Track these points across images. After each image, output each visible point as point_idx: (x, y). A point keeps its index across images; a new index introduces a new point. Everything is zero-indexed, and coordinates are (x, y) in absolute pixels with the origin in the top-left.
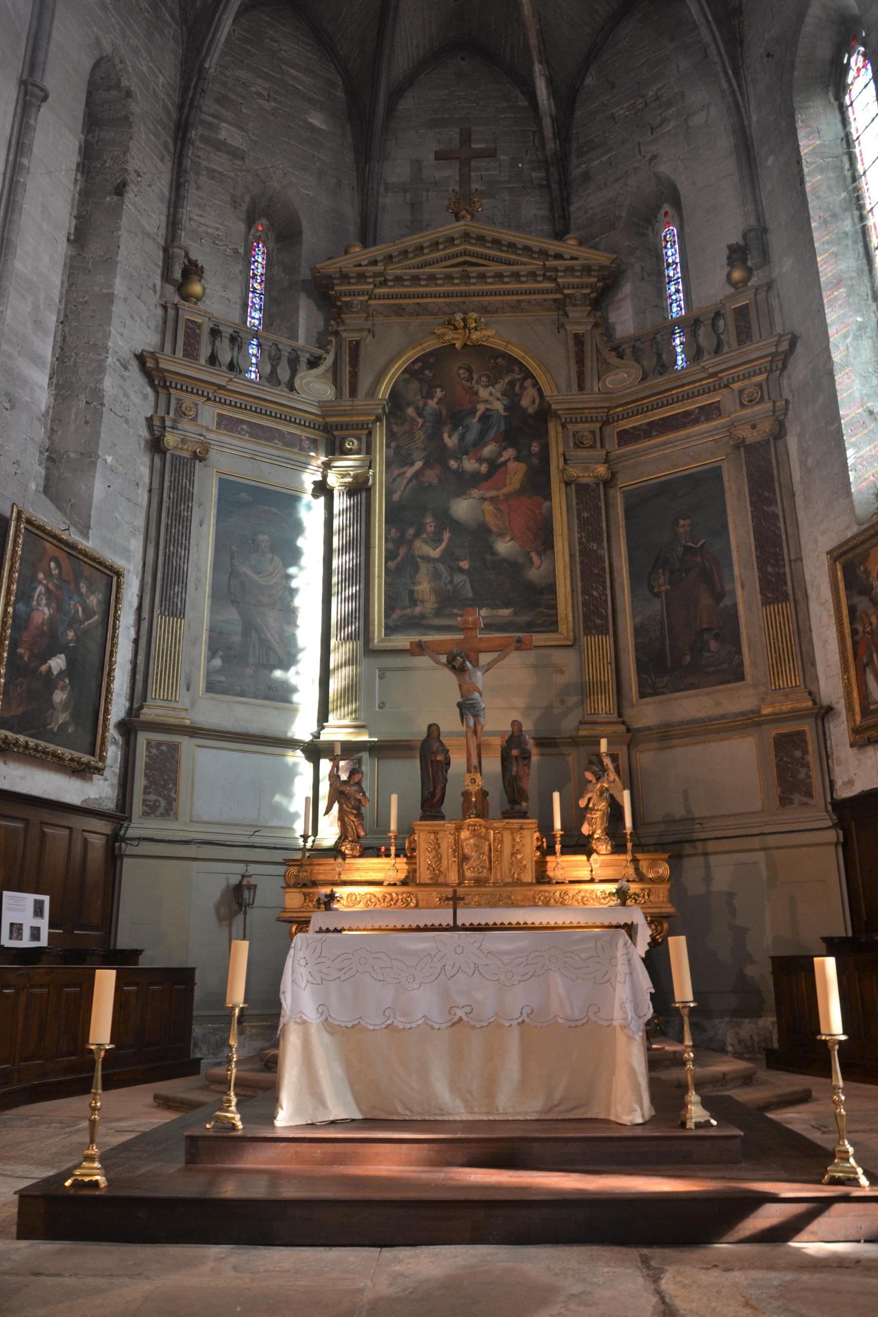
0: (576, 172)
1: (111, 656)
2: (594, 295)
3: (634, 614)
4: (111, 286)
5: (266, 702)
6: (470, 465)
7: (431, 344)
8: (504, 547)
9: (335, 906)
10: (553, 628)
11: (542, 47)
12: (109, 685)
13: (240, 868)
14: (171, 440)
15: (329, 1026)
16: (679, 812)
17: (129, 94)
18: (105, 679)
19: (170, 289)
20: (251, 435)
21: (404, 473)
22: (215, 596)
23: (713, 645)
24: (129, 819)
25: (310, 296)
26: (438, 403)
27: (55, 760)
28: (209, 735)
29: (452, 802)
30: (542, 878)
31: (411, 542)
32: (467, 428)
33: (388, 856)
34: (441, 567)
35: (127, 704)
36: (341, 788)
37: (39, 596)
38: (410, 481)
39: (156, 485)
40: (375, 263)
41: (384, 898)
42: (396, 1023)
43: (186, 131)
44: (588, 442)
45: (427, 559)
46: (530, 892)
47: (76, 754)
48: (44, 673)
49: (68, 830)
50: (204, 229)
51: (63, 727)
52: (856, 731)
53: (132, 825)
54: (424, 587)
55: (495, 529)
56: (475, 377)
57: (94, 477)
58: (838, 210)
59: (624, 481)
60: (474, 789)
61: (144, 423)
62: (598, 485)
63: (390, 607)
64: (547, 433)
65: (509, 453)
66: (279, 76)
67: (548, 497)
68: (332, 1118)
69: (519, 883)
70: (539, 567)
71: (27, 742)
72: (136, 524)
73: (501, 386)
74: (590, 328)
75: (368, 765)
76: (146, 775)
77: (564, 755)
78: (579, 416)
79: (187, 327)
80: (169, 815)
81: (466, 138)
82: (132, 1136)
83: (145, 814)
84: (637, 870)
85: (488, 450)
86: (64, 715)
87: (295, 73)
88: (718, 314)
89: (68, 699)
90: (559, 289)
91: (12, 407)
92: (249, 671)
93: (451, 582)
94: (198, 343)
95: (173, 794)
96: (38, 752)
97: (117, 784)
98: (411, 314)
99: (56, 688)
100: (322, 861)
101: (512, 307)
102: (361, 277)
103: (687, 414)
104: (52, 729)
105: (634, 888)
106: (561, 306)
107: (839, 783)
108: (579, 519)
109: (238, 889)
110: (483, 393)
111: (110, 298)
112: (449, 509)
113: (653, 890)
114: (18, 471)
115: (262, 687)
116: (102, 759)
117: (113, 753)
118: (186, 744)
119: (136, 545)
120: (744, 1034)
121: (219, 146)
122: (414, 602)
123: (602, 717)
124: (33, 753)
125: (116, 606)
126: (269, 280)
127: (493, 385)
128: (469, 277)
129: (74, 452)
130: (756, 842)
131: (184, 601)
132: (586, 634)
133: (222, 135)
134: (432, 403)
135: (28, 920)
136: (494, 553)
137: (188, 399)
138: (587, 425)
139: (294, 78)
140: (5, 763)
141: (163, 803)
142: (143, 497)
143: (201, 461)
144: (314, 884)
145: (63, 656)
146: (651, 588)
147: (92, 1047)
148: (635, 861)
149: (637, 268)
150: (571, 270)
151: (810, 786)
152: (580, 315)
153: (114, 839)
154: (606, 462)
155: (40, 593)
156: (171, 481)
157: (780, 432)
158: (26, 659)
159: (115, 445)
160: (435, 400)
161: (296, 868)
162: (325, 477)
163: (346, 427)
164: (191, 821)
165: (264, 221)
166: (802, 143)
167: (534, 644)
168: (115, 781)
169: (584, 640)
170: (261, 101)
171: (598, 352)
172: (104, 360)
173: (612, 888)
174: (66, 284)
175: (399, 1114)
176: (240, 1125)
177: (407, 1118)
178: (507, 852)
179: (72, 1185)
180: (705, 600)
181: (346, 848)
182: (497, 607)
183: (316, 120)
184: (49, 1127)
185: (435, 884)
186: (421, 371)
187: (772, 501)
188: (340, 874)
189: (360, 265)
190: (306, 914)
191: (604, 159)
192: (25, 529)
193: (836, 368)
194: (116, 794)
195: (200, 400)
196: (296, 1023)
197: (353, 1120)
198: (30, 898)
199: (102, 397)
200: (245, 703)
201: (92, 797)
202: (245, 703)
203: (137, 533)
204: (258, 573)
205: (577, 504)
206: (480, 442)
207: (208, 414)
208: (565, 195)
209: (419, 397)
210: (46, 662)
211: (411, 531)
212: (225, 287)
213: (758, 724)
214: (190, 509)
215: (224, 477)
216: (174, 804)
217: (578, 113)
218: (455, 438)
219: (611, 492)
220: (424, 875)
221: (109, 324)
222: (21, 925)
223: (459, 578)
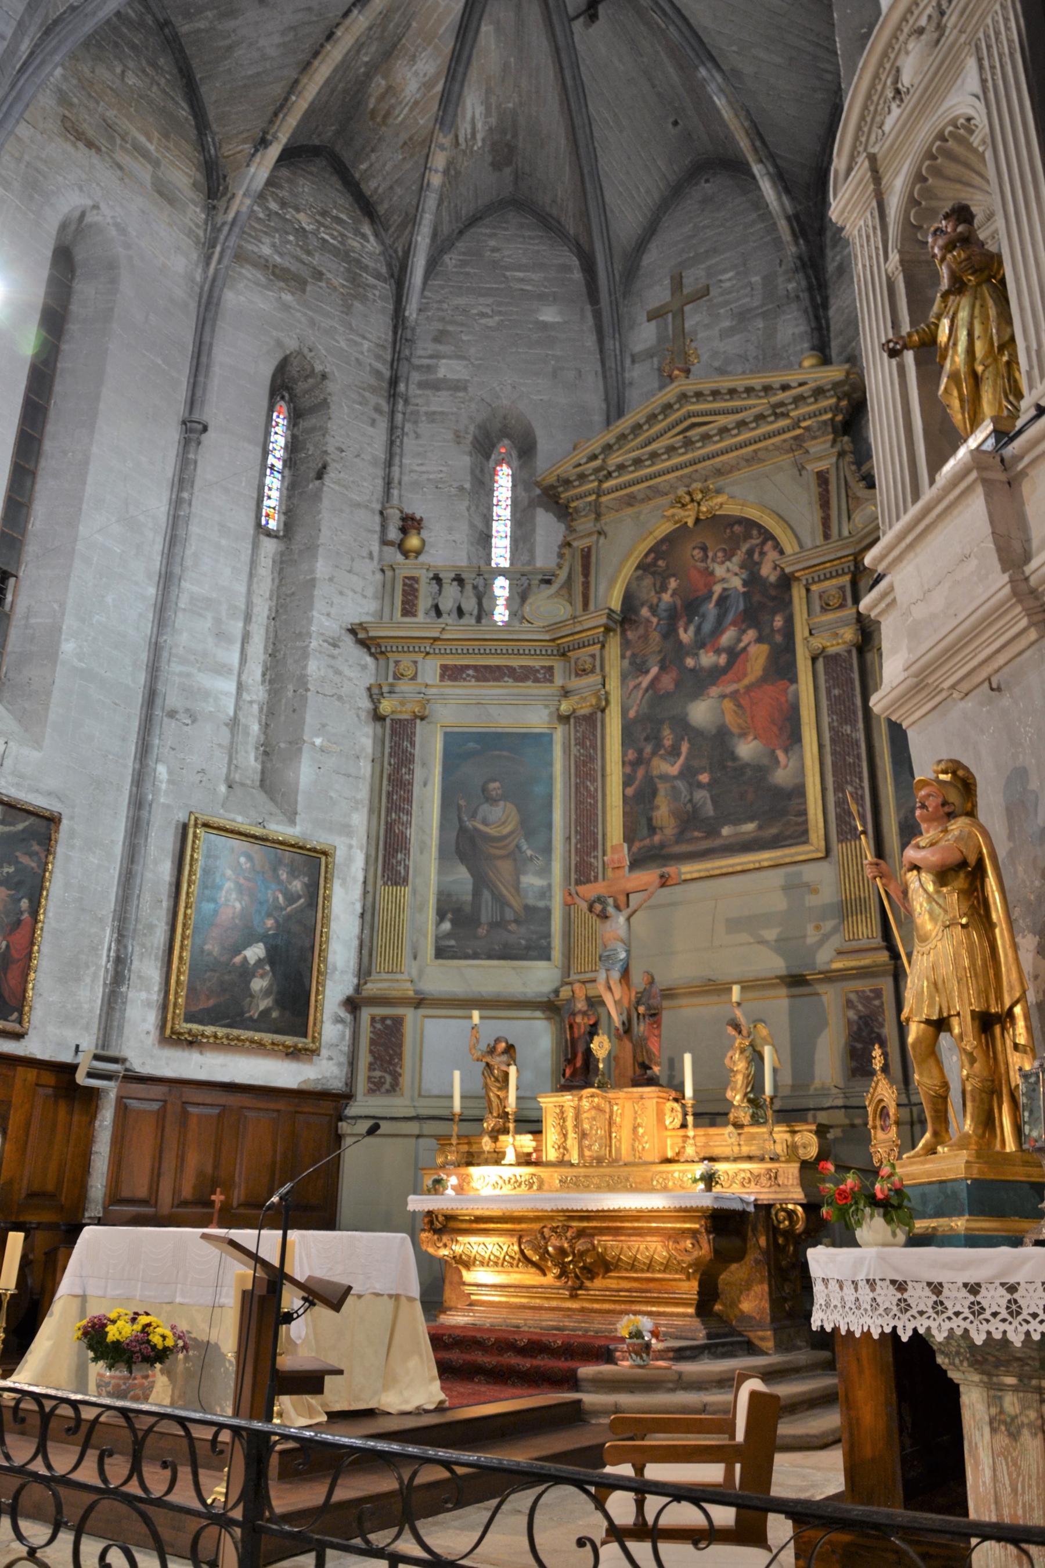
2: (839, 418)
4: (312, 571)
6: (707, 659)
8: (746, 749)
10: (803, 839)
11: (758, 144)
17: (324, 376)
20: (478, 680)
21: (640, 684)
26: (672, 596)
31: (649, 761)
32: (703, 616)
34: (680, 784)
38: (647, 690)
40: (594, 457)
45: (664, 777)
50: (425, 476)
51: (266, 1013)
55: (735, 730)
56: (710, 554)
61: (365, 694)
62: (849, 652)
64: (790, 602)
65: (751, 634)
66: (503, 286)
67: (794, 680)
70: (786, 766)
72: (359, 797)
74: (834, 460)
76: (371, 1051)
77: (818, 994)
78: (821, 573)
79: (405, 584)
83: (371, 1091)
85: (727, 637)
87: (520, 275)
89: (271, 985)
91: (193, 722)
93: (691, 801)
94: (416, 597)
98: (642, 501)
99: (254, 976)
101: (747, 460)
102: (582, 477)
104: (251, 1017)
108: (829, 698)
110: (720, 571)
111: (312, 583)
112: (687, 714)
113: (780, 1173)
118: (409, 1014)
121: (436, 386)
124: (225, 1042)
127: (729, 559)
128: (693, 443)
131: (406, 868)
132: (840, 841)
133: (442, 372)
134: (666, 597)
136: (734, 757)
137: (406, 660)
138: (834, 582)
139: (522, 280)
140: (201, 1053)
141: (389, 1079)
150: (799, 400)
152: (823, 447)
159: (324, 726)
160: (670, 592)
164: (420, 1095)
165: (506, 442)
167: (683, 877)
170: (484, 321)
172: (308, 646)
173: (699, 1169)
174: (277, 581)
185: (561, 1163)
186: (654, 563)
189: (580, 465)
195: (419, 657)
199: (306, 683)
205: (826, 681)
206: (718, 629)
208: (819, 300)
209: (653, 593)
211: (648, 749)
212: (450, 530)
214: (411, 772)
215: (449, 730)
218: (692, 629)
221: (311, 609)
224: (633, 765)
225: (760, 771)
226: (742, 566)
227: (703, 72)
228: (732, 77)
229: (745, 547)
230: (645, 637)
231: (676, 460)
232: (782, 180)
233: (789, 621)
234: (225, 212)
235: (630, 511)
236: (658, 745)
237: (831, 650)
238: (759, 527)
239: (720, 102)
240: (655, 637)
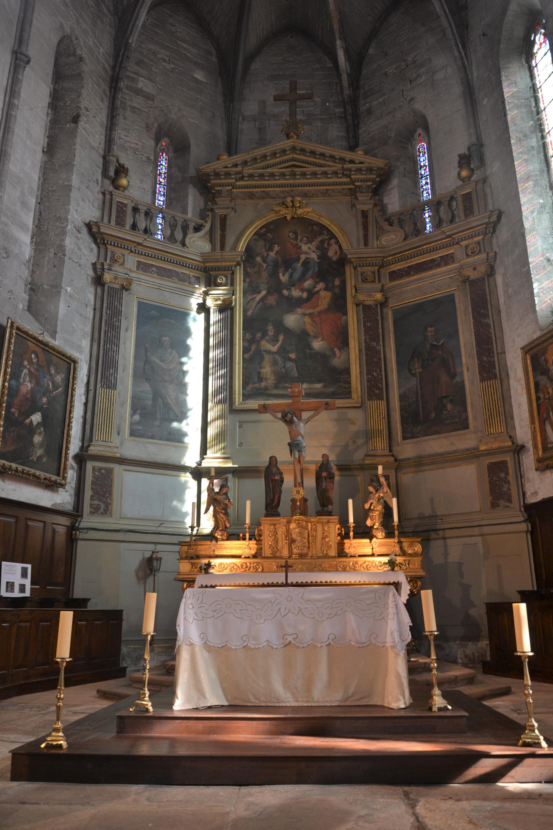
0: (363, 109)
1: (70, 413)
2: (374, 186)
3: (400, 387)
4: (70, 180)
5: (168, 443)
6: (296, 293)
7: (272, 217)
8: (317, 345)
9: (211, 571)
10: (348, 396)
11: (341, 29)
12: (68, 432)
13: (151, 547)
14: (107, 277)
15: (207, 646)
16: (428, 512)
17: (81, 59)
18: (66, 428)
19: (107, 182)
20: (158, 274)
21: (255, 298)
22: (136, 375)
23: (449, 406)
24: (81, 516)
25: (195, 186)
26: (276, 254)
27: (35, 479)
28: (132, 463)
29: (285, 506)
30: (342, 553)
31: (259, 342)
32: (294, 270)
33: (244, 539)
34: (278, 357)
35: (80, 444)
36: (215, 497)
37: (24, 376)
38: (258, 303)
39: (98, 306)
40: (236, 165)
41: (242, 566)
42: (249, 645)
43: (117, 82)
44: (370, 279)
45: (269, 352)
46: (334, 562)
47: (48, 475)
48: (27, 424)
49: (43, 523)
50: (129, 144)
51: (40, 458)
52: (539, 461)
53: (83, 520)
54: (267, 370)
55: (312, 334)
56: (299, 237)
57: (59, 300)
58: (528, 132)
59: (393, 303)
60: (298, 497)
61: (90, 266)
62: (376, 305)
63: (245, 383)
64: (344, 273)
65: (321, 285)
66: (176, 48)
67: (345, 313)
68: (209, 705)
69: (327, 557)
70: (340, 357)
71: (17, 468)
72: (86, 330)
73: (315, 243)
74: (371, 206)
75: (232, 482)
76: (92, 489)
77: (355, 476)
78: (364, 262)
79: (118, 206)
80: (106, 514)
81: (293, 87)
82: (83, 716)
83: (92, 513)
84: (401, 548)
85: (308, 284)
86: (40, 451)
87: (186, 46)
88: (452, 198)
89: (43, 440)
90: (352, 182)
91: (8, 257)
92: (157, 423)
93: (284, 367)
94: (125, 216)
95: (109, 501)
96: (24, 474)
97: (74, 494)
98: (259, 198)
99: (35, 434)
100: (203, 543)
101: (322, 193)
102: (228, 174)
103: (433, 261)
104: (33, 460)
105: (399, 559)
106: (353, 193)
107: (528, 493)
108: (365, 327)
109: (150, 560)
110: (304, 248)
111: (69, 188)
112: (283, 321)
113: (411, 561)
114: (11, 297)
115: (165, 433)
116: (64, 478)
117: (71, 475)
118: (117, 469)
119: (86, 343)
120: (468, 651)
121: (138, 92)
122: (261, 379)
123: (379, 452)
124: (21, 475)
125: (73, 382)
126: (169, 177)
127: (310, 243)
128: (295, 175)
129: (47, 285)
130: (476, 531)
131: (116, 379)
132: (369, 400)
133: (140, 85)
134: (272, 254)
135: (18, 580)
136: (311, 349)
137: (118, 252)
138: (370, 268)
139: (185, 49)
140: (3, 481)
141: (103, 506)
142: (90, 314)
143: (126, 291)
144: (198, 557)
145: (39, 414)
146: (410, 371)
147: (58, 660)
148: (400, 542)
149: (401, 169)
150: (359, 170)
151: (510, 495)
152: (365, 198)
153: (72, 529)
154: (382, 291)
155: (25, 374)
156: (107, 303)
157: (491, 272)
158: (16, 415)
159: (72, 281)
160: (274, 252)
161: (186, 547)
162: (204, 300)
163: (218, 269)
164: (120, 517)
165: (166, 139)
166: (505, 90)
167: (337, 406)
168: (73, 492)
169: (368, 403)
170: (164, 64)
171: (377, 222)
172: (66, 227)
173: (386, 559)
174: (42, 179)
175: (251, 702)
176: (151, 709)
177: (256, 705)
178: (319, 537)
179: (45, 747)
180: (444, 378)
181: (218, 535)
182: (313, 382)
183: (199, 75)
184: (31, 711)
185: (274, 557)
186: (265, 234)
187: (486, 316)
188: (214, 551)
189: (227, 167)
190: (193, 576)
191: (380, 100)
192: (16, 333)
193: (527, 232)
194: (73, 501)
195: (126, 252)
196: (186, 644)
197: (222, 706)
198: (19, 566)
199: (65, 250)
200: (155, 443)
201: (58, 502)
202: (155, 443)
203: (86, 336)
204: (162, 361)
205: (364, 318)
206: (302, 278)
207: (131, 261)
208: (356, 123)
209: (264, 250)
210: (29, 417)
211: (259, 335)
212: (142, 181)
213: (478, 457)
214: (120, 321)
215: (141, 300)
216: (110, 506)
217: (364, 71)
218: (287, 276)
219: (385, 310)
220: (267, 552)
221: (69, 204)
222: (13, 583)
223: (289, 364)
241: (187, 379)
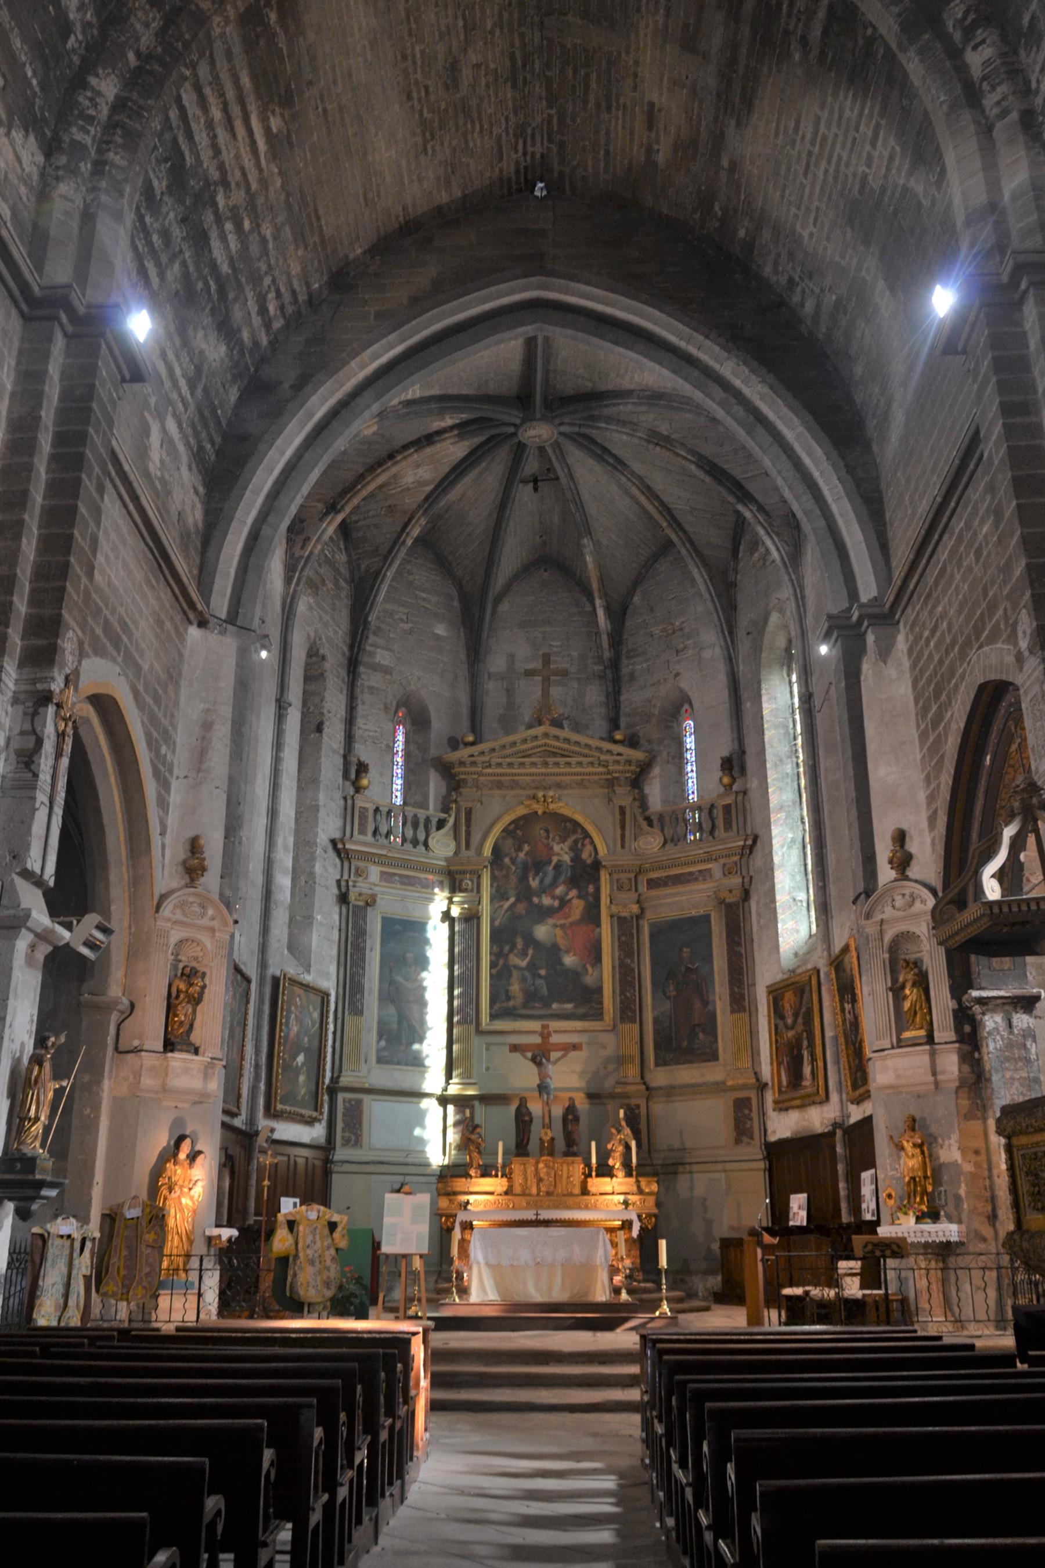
0: (625, 671)
3: (654, 1008)
4: (317, 800)
6: (547, 901)
7: (521, 811)
8: (569, 960)
13: (400, 1178)
14: (352, 896)
15: (488, 1265)
16: (677, 1145)
19: (348, 784)
22: (381, 998)
23: (701, 1036)
24: (334, 1149)
25: (437, 770)
29: (533, 1145)
30: (585, 1191)
32: (545, 873)
33: (496, 1176)
34: (527, 974)
43: (355, 667)
44: (626, 886)
46: (577, 1200)
52: (775, 1102)
54: (515, 987)
58: (784, 757)
59: (649, 915)
60: (547, 1138)
61: (334, 884)
63: (493, 1002)
64: (599, 879)
65: (574, 893)
69: (571, 1194)
73: (569, 842)
75: (480, 1110)
81: (546, 659)
83: (343, 1145)
84: (639, 1187)
85: (560, 890)
87: (424, 595)
88: (712, 806)
90: (609, 773)
92: (402, 1048)
103: (691, 874)
105: (632, 1198)
107: (769, 1132)
110: (557, 848)
118: (366, 1099)
119: (333, 969)
120: (709, 1285)
123: (630, 1080)
126: (407, 755)
130: (720, 1166)
134: (522, 855)
136: (561, 963)
137: (362, 864)
139: (424, 600)
146: (664, 993)
148: (638, 1182)
149: (665, 754)
151: (752, 1133)
153: (327, 1161)
154: (638, 902)
157: (746, 895)
162: (449, 909)
163: (464, 872)
166: (765, 705)
169: (620, 1026)
171: (635, 820)
173: (621, 1198)
178: (565, 1176)
180: (697, 1005)
182: (564, 1002)
183: (440, 630)
185: (524, 1194)
186: (514, 831)
187: (739, 944)
191: (645, 665)
193: (776, 867)
204: (407, 980)
206: (554, 884)
207: (374, 872)
211: (507, 948)
213: (725, 1091)
214: (365, 941)
217: (628, 624)
219: (641, 922)
220: (517, 1189)
223: (539, 982)
224: (497, 956)
225: (575, 975)
226: (571, 849)
227: (585, 541)
228: (597, 544)
229: (573, 838)
230: (507, 877)
231: (533, 770)
232: (608, 609)
233: (598, 890)
234: (302, 548)
235: (498, 792)
236: (513, 946)
237: (623, 914)
238: (583, 828)
239: (589, 559)
240: (514, 879)
241: (428, 996)
